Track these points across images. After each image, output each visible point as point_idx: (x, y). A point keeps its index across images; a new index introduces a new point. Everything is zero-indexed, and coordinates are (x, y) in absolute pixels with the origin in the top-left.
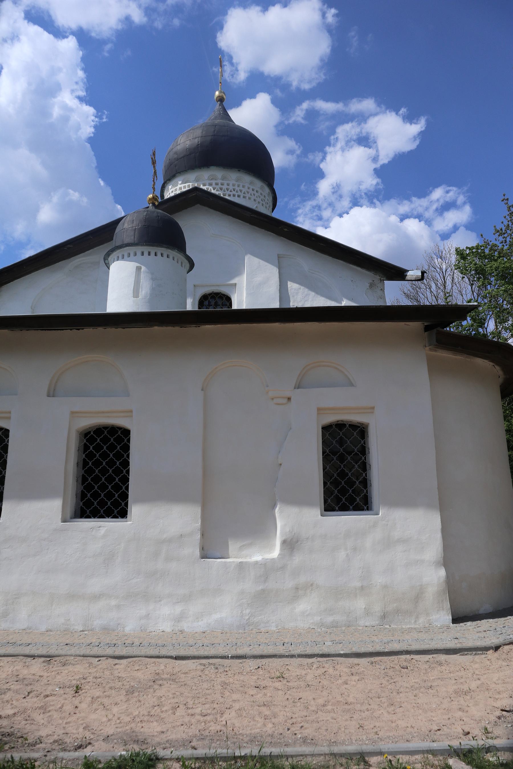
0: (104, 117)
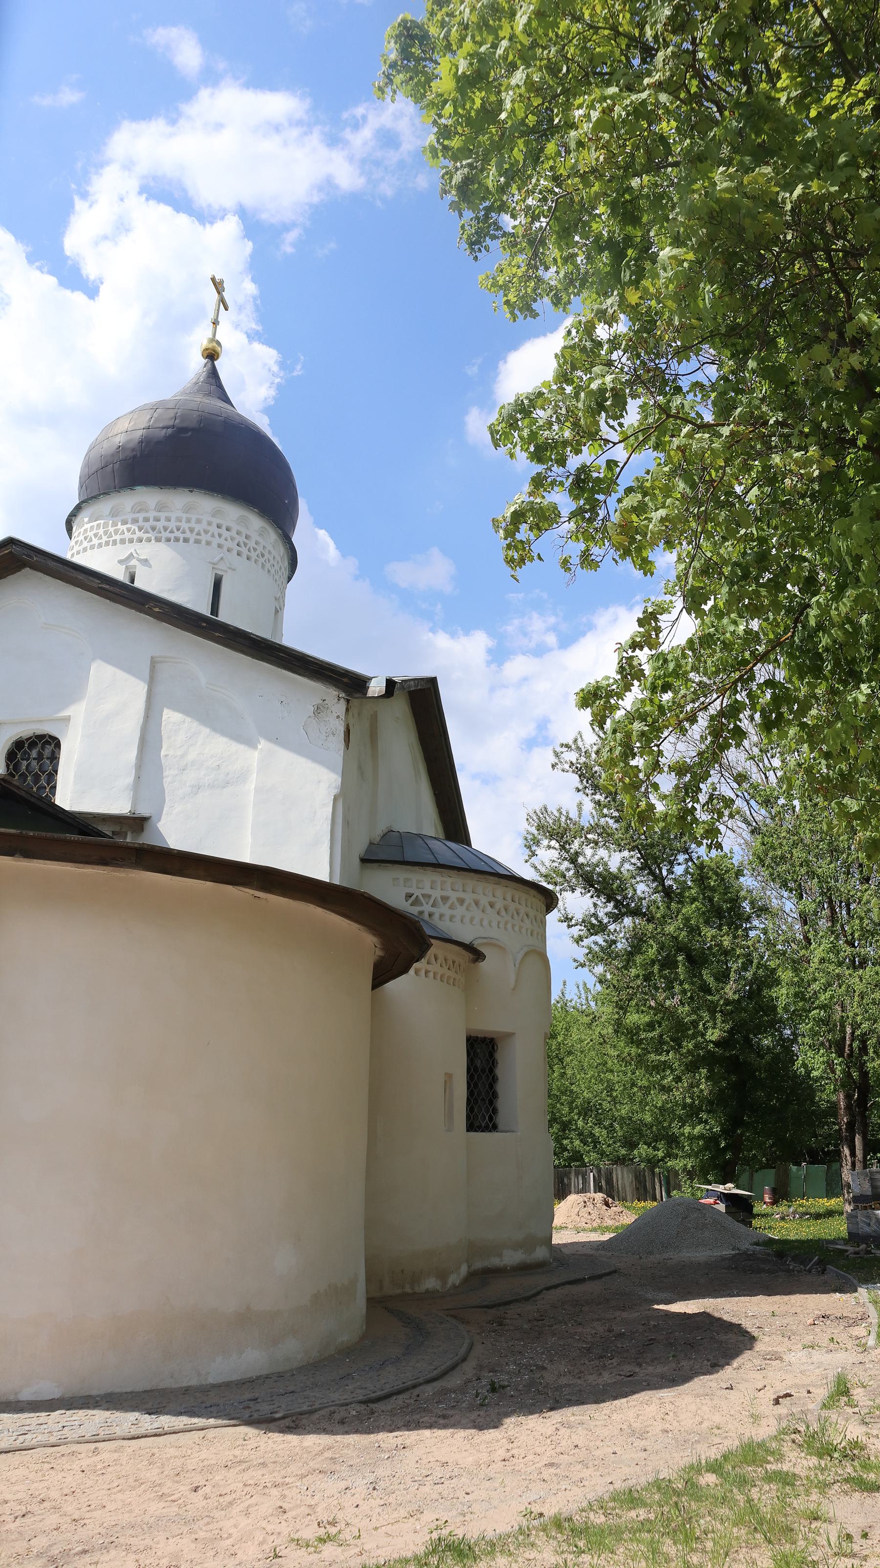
0: (299, 367)
